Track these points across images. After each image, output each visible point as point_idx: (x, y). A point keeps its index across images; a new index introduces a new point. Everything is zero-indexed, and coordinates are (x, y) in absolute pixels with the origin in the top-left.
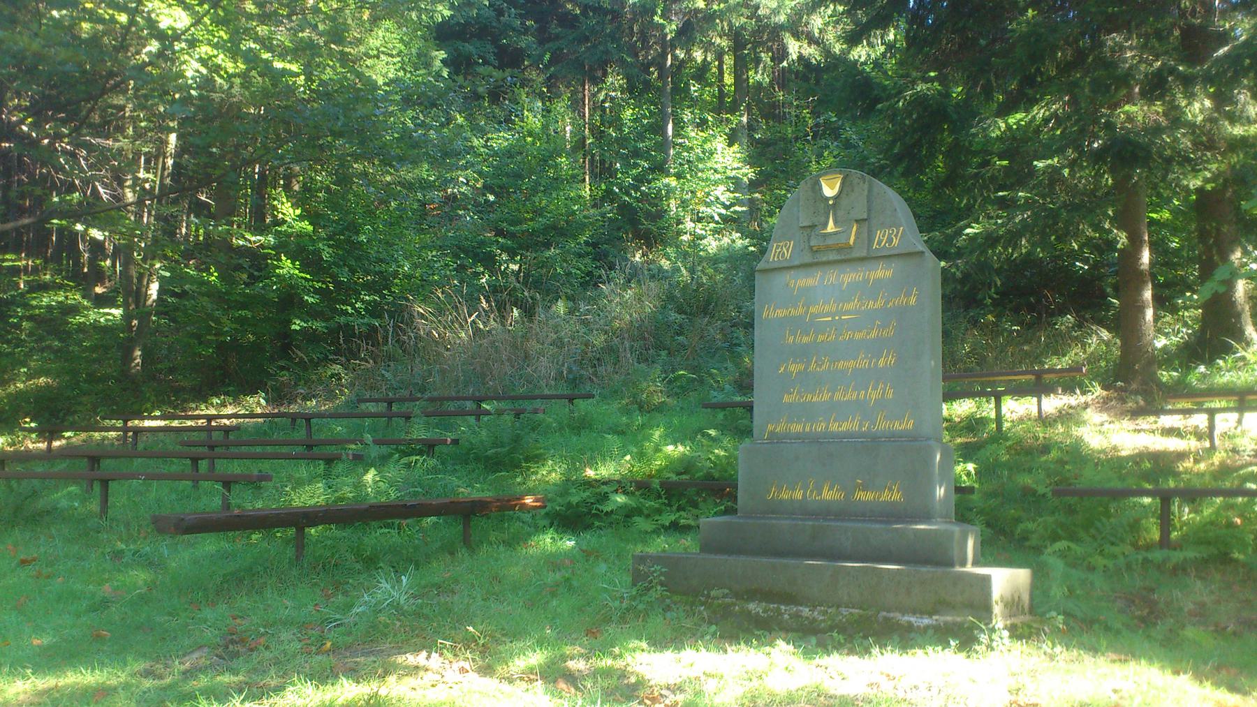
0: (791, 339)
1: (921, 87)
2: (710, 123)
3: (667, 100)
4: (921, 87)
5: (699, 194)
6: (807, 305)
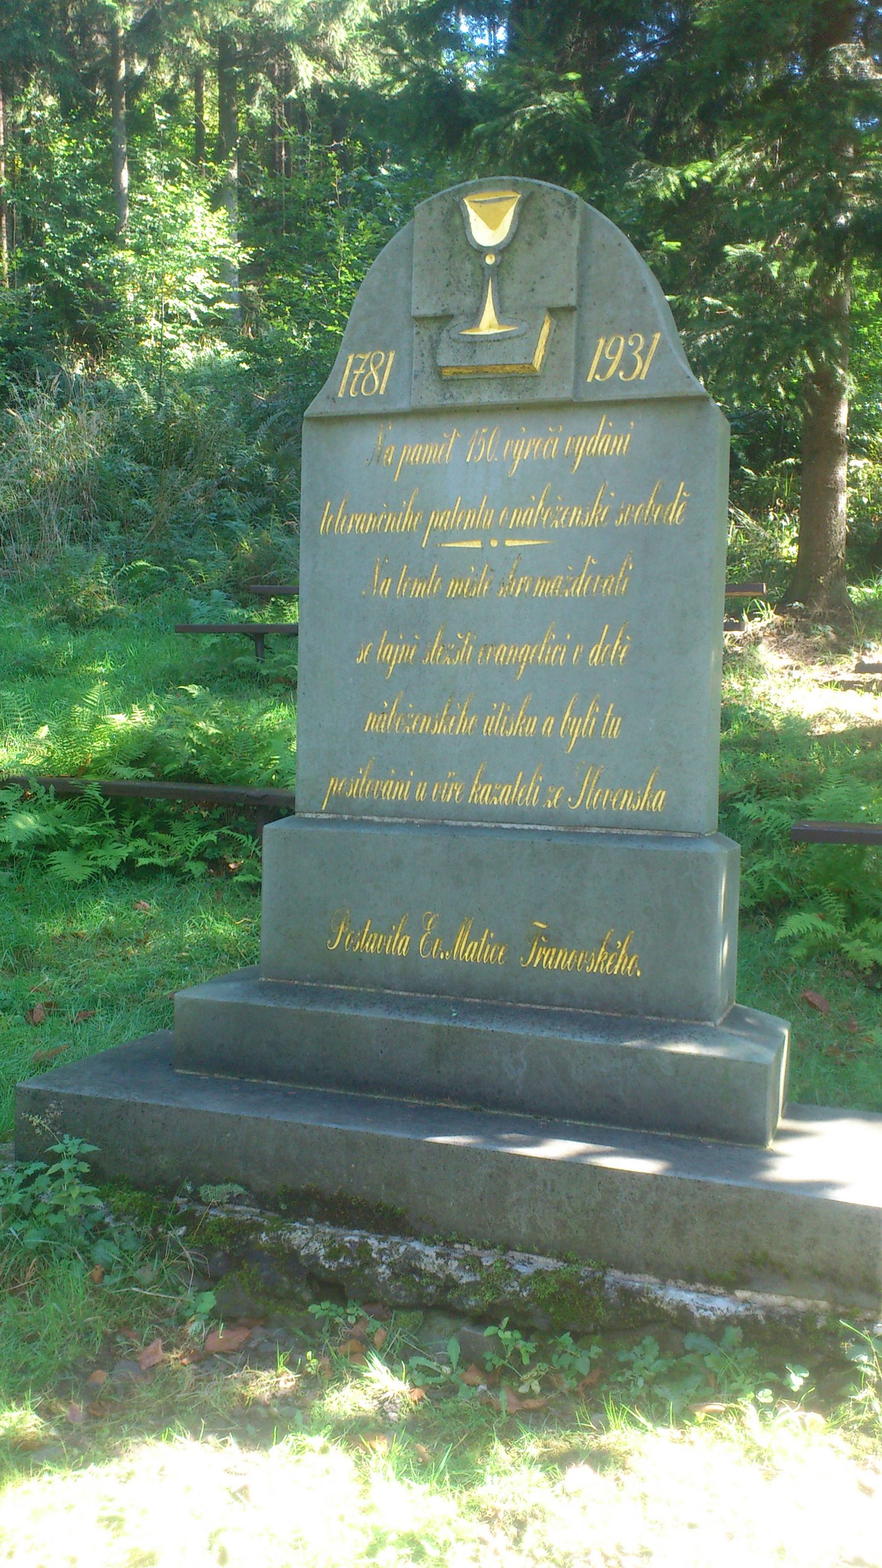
0: (385, 588)
1: (553, 99)
2: (184, 174)
3: (119, 131)
4: (553, 99)
5: (169, 280)
6: (425, 509)
